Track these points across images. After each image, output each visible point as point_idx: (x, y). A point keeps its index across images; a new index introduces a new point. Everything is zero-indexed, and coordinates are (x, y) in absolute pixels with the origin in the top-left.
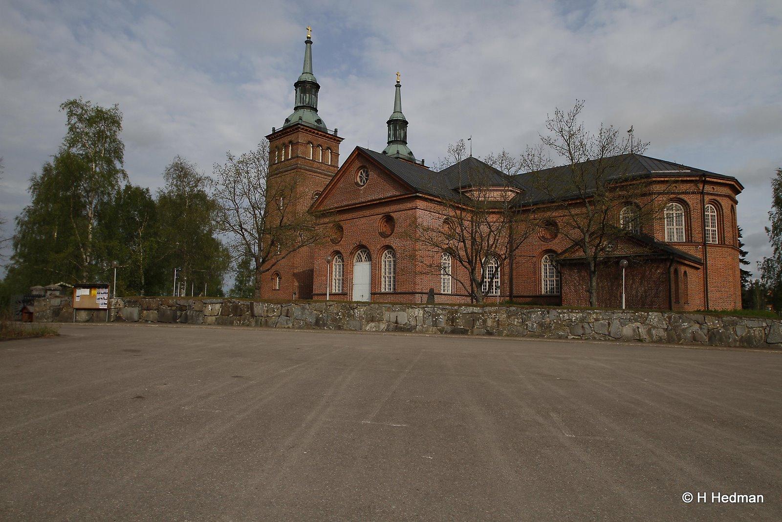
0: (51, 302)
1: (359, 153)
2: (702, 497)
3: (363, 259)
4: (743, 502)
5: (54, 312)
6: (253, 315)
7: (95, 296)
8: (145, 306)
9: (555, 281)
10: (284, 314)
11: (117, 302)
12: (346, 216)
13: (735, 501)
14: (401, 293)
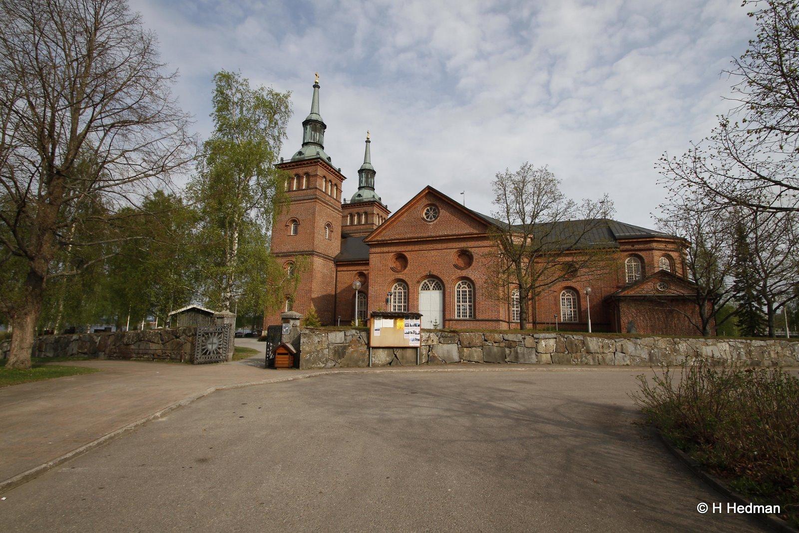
0: (329, 337)
1: (429, 192)
3: (431, 288)
4: (759, 512)
5: (335, 351)
6: (588, 352)
7: (401, 329)
8: (466, 343)
9: (403, 307)
10: (619, 350)
11: (429, 337)
12: (410, 248)
13: (751, 512)
14: (482, 320)
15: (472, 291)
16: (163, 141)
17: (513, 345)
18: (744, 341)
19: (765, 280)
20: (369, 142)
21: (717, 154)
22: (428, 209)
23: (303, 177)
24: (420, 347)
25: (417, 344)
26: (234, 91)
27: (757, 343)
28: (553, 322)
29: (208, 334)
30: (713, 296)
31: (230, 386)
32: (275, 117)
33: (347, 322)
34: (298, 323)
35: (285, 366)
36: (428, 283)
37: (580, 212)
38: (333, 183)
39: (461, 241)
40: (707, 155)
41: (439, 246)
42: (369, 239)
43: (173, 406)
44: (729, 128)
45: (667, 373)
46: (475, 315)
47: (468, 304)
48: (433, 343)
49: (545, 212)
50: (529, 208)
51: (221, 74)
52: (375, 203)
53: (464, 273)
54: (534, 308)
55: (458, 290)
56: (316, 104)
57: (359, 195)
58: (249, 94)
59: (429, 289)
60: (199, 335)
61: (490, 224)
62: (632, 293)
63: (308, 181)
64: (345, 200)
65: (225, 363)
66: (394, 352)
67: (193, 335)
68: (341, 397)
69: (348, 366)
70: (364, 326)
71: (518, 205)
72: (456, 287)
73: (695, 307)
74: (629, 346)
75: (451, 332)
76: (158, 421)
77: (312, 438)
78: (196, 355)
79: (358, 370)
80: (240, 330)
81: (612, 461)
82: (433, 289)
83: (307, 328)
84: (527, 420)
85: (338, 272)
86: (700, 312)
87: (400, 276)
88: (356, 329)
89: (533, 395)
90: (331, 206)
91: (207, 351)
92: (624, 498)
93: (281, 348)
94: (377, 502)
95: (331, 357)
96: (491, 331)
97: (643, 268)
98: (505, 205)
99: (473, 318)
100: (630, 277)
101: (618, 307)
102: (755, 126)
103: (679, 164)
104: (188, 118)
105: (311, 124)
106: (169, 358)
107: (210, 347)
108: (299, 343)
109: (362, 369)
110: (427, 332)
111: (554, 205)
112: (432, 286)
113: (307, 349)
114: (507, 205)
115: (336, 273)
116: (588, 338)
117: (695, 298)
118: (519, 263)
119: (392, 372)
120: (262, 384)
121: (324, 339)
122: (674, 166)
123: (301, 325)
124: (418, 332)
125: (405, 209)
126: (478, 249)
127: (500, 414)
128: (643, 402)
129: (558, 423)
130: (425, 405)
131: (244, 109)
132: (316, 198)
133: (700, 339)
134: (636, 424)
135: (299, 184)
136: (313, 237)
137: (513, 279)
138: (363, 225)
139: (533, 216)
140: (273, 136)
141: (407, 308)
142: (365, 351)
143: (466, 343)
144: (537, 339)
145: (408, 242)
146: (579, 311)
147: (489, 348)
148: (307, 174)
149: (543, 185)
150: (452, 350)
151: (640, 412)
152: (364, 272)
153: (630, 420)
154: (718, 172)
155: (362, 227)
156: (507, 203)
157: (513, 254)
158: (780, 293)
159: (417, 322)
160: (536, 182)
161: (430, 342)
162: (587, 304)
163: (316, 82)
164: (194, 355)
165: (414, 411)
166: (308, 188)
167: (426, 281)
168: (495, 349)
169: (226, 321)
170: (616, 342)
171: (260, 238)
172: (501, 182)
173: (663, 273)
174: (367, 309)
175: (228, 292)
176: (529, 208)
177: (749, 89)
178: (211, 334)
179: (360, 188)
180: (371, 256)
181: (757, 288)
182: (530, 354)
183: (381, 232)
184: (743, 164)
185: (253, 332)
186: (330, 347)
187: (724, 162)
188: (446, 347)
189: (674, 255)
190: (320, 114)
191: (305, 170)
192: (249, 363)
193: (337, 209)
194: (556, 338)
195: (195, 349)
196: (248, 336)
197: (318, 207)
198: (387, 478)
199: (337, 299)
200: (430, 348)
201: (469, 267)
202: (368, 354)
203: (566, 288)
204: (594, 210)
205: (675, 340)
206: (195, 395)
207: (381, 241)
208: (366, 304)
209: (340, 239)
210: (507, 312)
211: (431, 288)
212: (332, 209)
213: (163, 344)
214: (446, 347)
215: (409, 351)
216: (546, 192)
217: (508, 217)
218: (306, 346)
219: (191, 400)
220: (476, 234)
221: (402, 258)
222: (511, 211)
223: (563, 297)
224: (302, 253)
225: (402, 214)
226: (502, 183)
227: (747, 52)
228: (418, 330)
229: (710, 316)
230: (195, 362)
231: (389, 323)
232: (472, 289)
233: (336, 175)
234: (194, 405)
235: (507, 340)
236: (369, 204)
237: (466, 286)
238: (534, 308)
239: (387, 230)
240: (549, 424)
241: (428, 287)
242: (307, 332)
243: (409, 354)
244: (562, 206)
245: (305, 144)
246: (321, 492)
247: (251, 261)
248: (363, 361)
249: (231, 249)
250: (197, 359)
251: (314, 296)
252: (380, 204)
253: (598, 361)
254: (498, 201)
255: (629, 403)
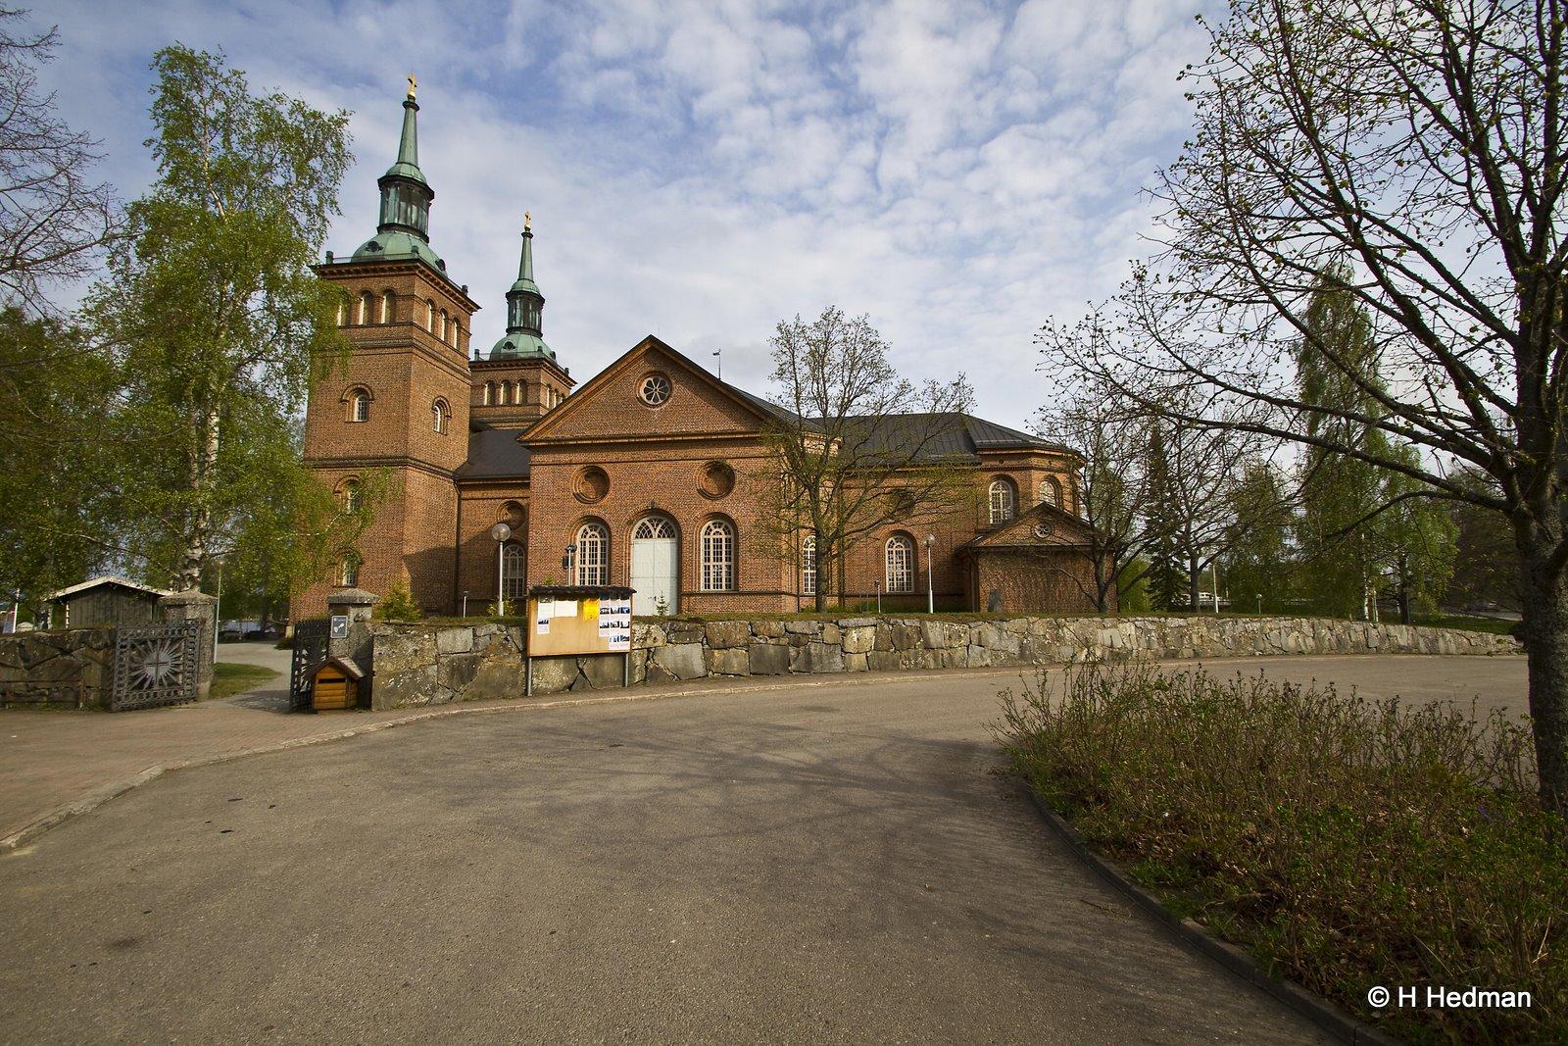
0: (440, 642)
2: (1407, 996)
3: (655, 534)
4: (1489, 1005)
5: (453, 669)
6: (928, 647)
8: (718, 640)
9: (599, 570)
10: (975, 641)
12: (613, 456)
13: (1473, 1004)
15: (732, 540)
16: (15, 195)
17: (803, 640)
18: (1156, 619)
19: (1188, 521)
20: (531, 236)
21: (1127, 326)
22: (650, 381)
23: (380, 299)
24: (630, 653)
25: (624, 647)
26: (207, 93)
27: (1175, 622)
28: (873, 592)
29: (145, 642)
30: (1116, 547)
31: (202, 760)
32: (310, 163)
33: (481, 606)
34: (367, 613)
35: (336, 705)
36: (648, 524)
37: (919, 402)
38: (450, 316)
39: (713, 446)
40: (1112, 327)
41: (671, 454)
42: (530, 436)
43: (50, 819)
44: (1146, 284)
45: (1044, 684)
46: (736, 584)
47: (724, 563)
48: (656, 644)
49: (861, 399)
50: (834, 391)
51: (175, 53)
52: (544, 362)
53: (717, 506)
54: (841, 572)
55: (707, 537)
56: (410, 143)
57: (509, 345)
58: (246, 106)
59: (651, 537)
60: (122, 647)
61: (768, 415)
62: (995, 541)
63: (392, 307)
64: (477, 352)
65: (192, 705)
66: (578, 664)
67: (106, 645)
68: (462, 766)
69: (481, 697)
70: (516, 614)
71: (815, 385)
72: (702, 532)
73: (1089, 564)
74: (989, 633)
75: (690, 620)
76: (9, 856)
77: (392, 864)
78: (115, 693)
79: (502, 706)
80: (233, 624)
81: (956, 847)
82: (659, 536)
83: (389, 624)
84: (820, 784)
85: (462, 502)
86: (1096, 574)
87: (594, 511)
88: (498, 621)
89: (833, 734)
90: (447, 365)
91: (145, 680)
92: (973, 913)
93: (328, 669)
94: (528, 989)
95: (444, 680)
96: (765, 617)
97: (1016, 500)
98: (793, 383)
99: (734, 589)
100: (996, 514)
101: (977, 565)
102: (1184, 287)
103: (1070, 339)
104: (83, 146)
105: (399, 185)
106: (45, 699)
107: (151, 671)
108: (371, 656)
109: (513, 702)
110: (645, 623)
111: (877, 388)
112: (658, 530)
113: (389, 667)
114: (797, 383)
115: (459, 504)
116: (928, 624)
117: (1088, 549)
118: (817, 491)
119: (574, 705)
120: (280, 751)
121: (428, 645)
122: (1063, 342)
123: (374, 616)
124: (625, 624)
125: (604, 380)
126: (747, 462)
127: (775, 775)
128: (1006, 732)
129: (874, 784)
130: (636, 770)
131: (234, 138)
132: (412, 345)
133: (1094, 619)
134: (995, 774)
135: (372, 311)
136: (406, 428)
137: (805, 519)
138: (518, 405)
139: (842, 405)
140: (306, 206)
141: (607, 574)
142: (519, 666)
143: (718, 640)
144: (843, 628)
145: (610, 444)
146: (915, 573)
147: (761, 648)
148: (390, 293)
149: (859, 351)
150: (693, 654)
151: (1003, 752)
152: (520, 501)
153: (987, 768)
154: (1128, 356)
155: (515, 410)
156: (796, 380)
157: (806, 472)
158: (1209, 542)
159: (626, 604)
160: (849, 345)
161: (649, 642)
162: (927, 562)
163: (409, 96)
164: (111, 690)
165: (615, 784)
166: (392, 322)
167: (645, 520)
168: (771, 650)
169: (191, 614)
170: (970, 627)
171: (274, 427)
172: (786, 338)
173: (1045, 508)
174: (526, 577)
175: (197, 548)
176: (834, 391)
177: (1179, 224)
178: (154, 642)
179: (510, 330)
180: (534, 471)
181: (1178, 533)
182: (832, 654)
183: (554, 423)
184: (1164, 344)
185: (264, 628)
186: (442, 660)
187: (1137, 340)
188: (680, 649)
189: (1061, 478)
190: (419, 166)
191: (386, 283)
192: (251, 703)
193: (458, 371)
194: (875, 626)
195: (112, 678)
196: (251, 637)
197: (417, 363)
198: (552, 933)
199: (462, 557)
200: (650, 653)
201: (728, 494)
202: (524, 670)
203: (895, 533)
204: (943, 400)
205: (1059, 620)
206: (111, 786)
207: (554, 441)
208: (524, 565)
209: (467, 432)
210: (794, 578)
211: (655, 534)
212: (449, 370)
213: (28, 669)
214: (680, 650)
215: (609, 663)
216: (864, 364)
217: (798, 406)
218: (385, 662)
219: (99, 800)
220: (740, 433)
221: (597, 476)
222: (804, 395)
223: (890, 549)
224: (378, 462)
225: (598, 389)
226: (788, 342)
227: (1180, 160)
228: (626, 619)
229: (1109, 582)
230: (114, 706)
231: (568, 608)
232: (732, 537)
233: (457, 298)
234: (108, 812)
235: (792, 633)
236: (530, 364)
237: (721, 530)
238: (841, 572)
239: (567, 418)
240: (858, 786)
241: (650, 532)
242: (389, 631)
243: (609, 667)
244: (891, 391)
245: (383, 228)
246: (406, 985)
247: (252, 482)
248: (514, 685)
249: (202, 450)
250: (119, 699)
251: (409, 550)
252: (555, 366)
253: (942, 660)
254: (781, 374)
255: (984, 737)
